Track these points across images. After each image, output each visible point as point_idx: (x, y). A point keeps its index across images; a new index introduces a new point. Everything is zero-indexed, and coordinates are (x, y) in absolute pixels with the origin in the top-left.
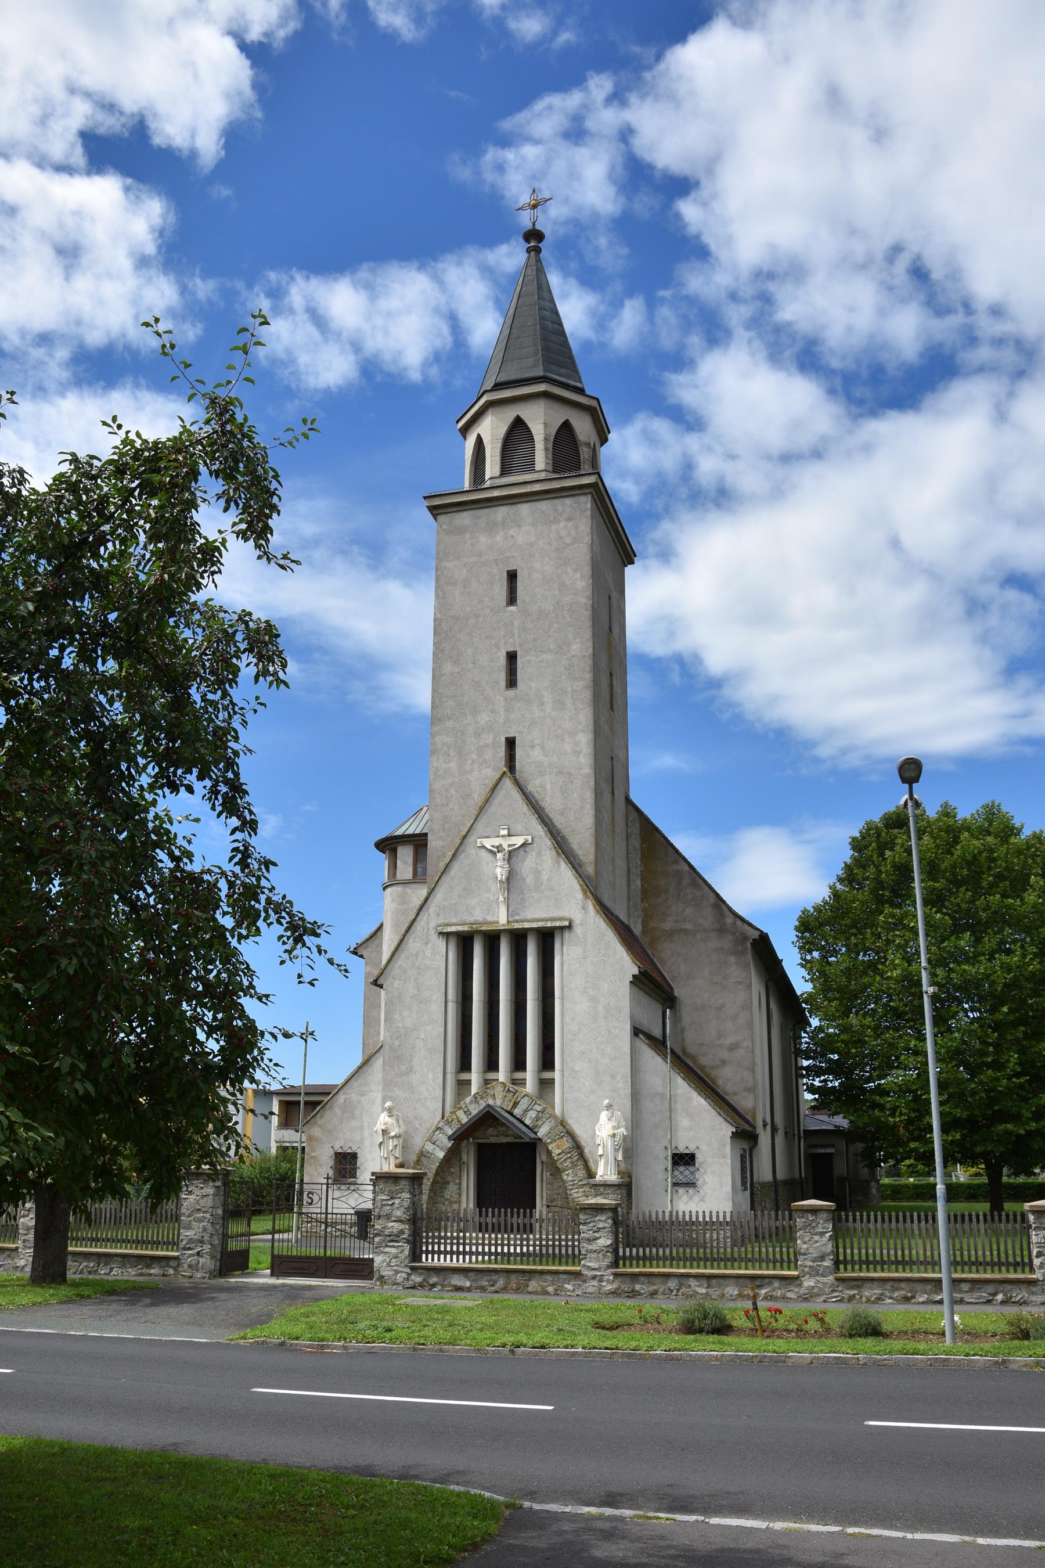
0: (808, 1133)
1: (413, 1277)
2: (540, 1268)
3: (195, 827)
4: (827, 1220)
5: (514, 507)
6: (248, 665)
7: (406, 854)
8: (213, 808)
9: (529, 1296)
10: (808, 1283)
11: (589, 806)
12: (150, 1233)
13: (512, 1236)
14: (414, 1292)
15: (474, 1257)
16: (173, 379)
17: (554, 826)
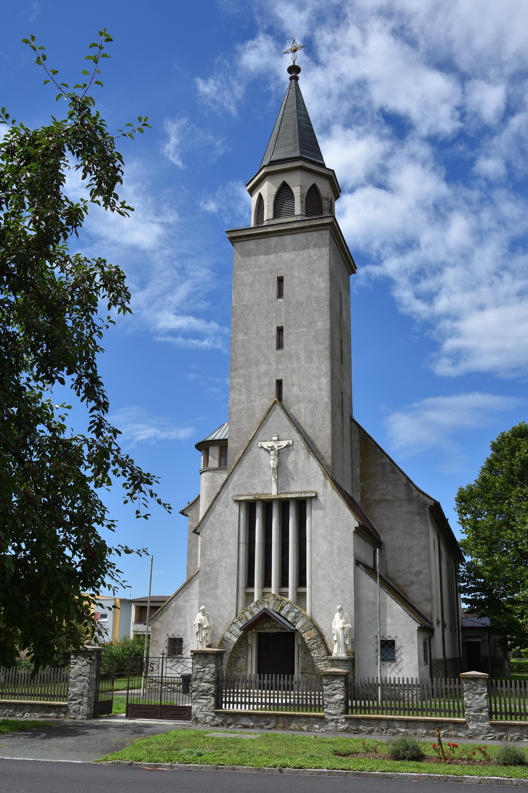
0: (464, 628)
1: (217, 719)
2: (298, 713)
3: (62, 401)
4: (483, 686)
5: (282, 238)
6: (103, 297)
7: (214, 452)
8: (78, 394)
9: (291, 732)
10: (472, 726)
11: (328, 422)
12: (32, 690)
13: (280, 692)
14: (217, 728)
15: (255, 706)
16: (45, 83)
17: (306, 435)
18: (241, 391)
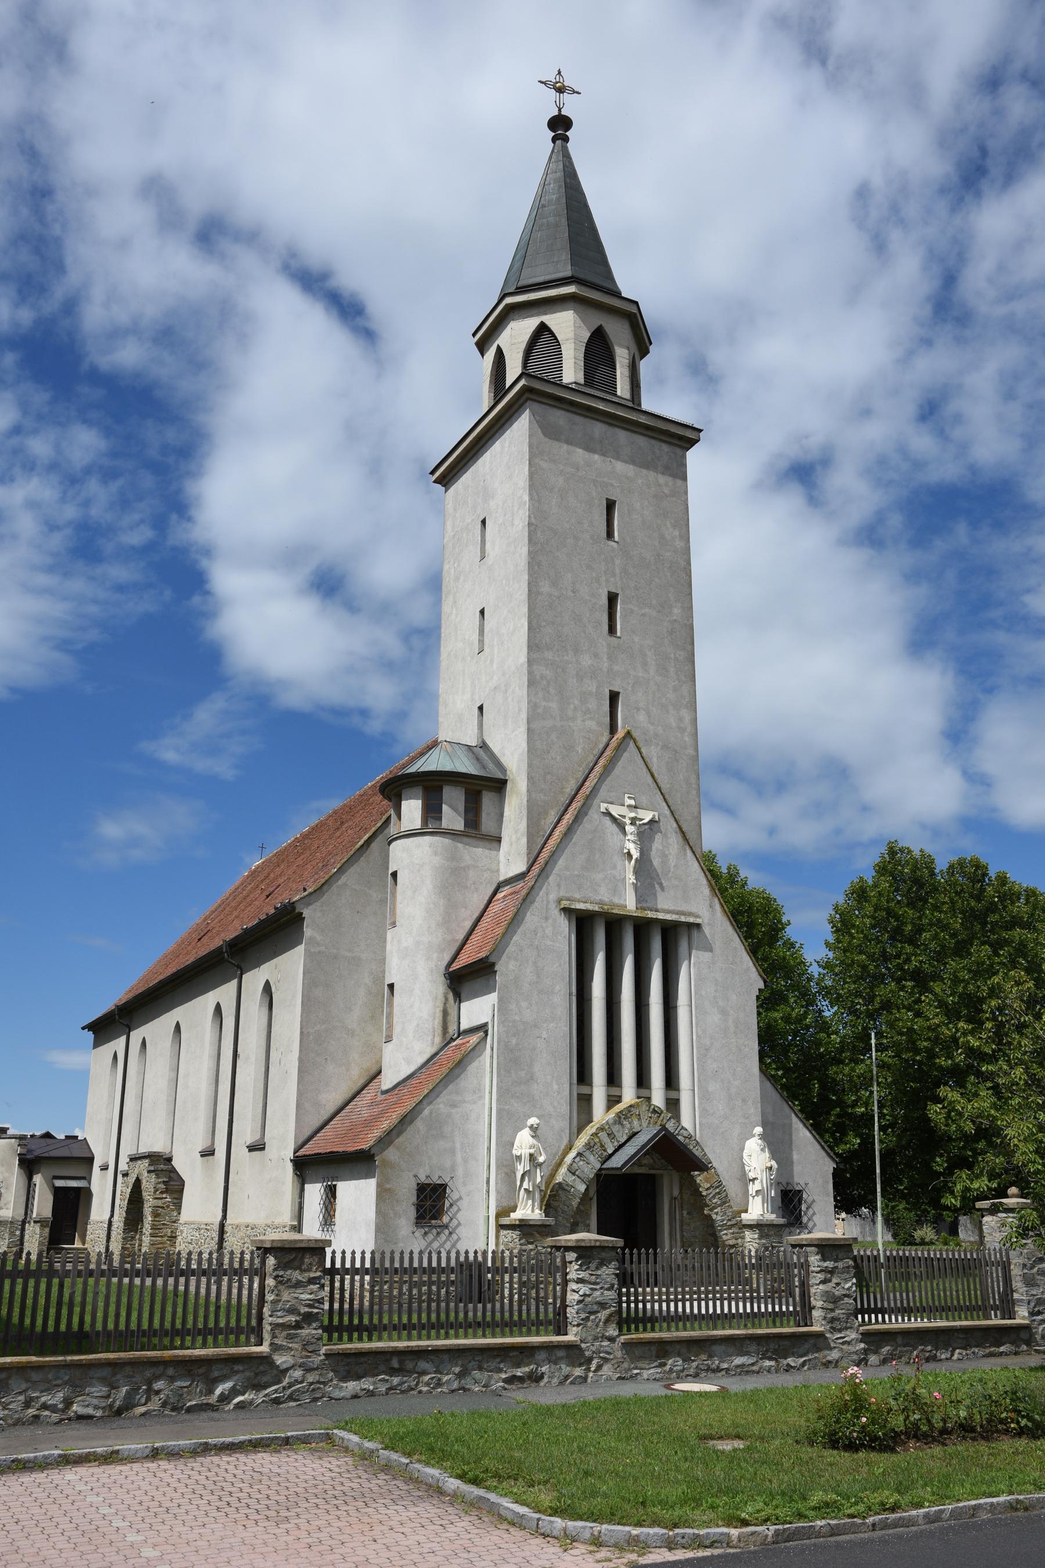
18: (548, 692)
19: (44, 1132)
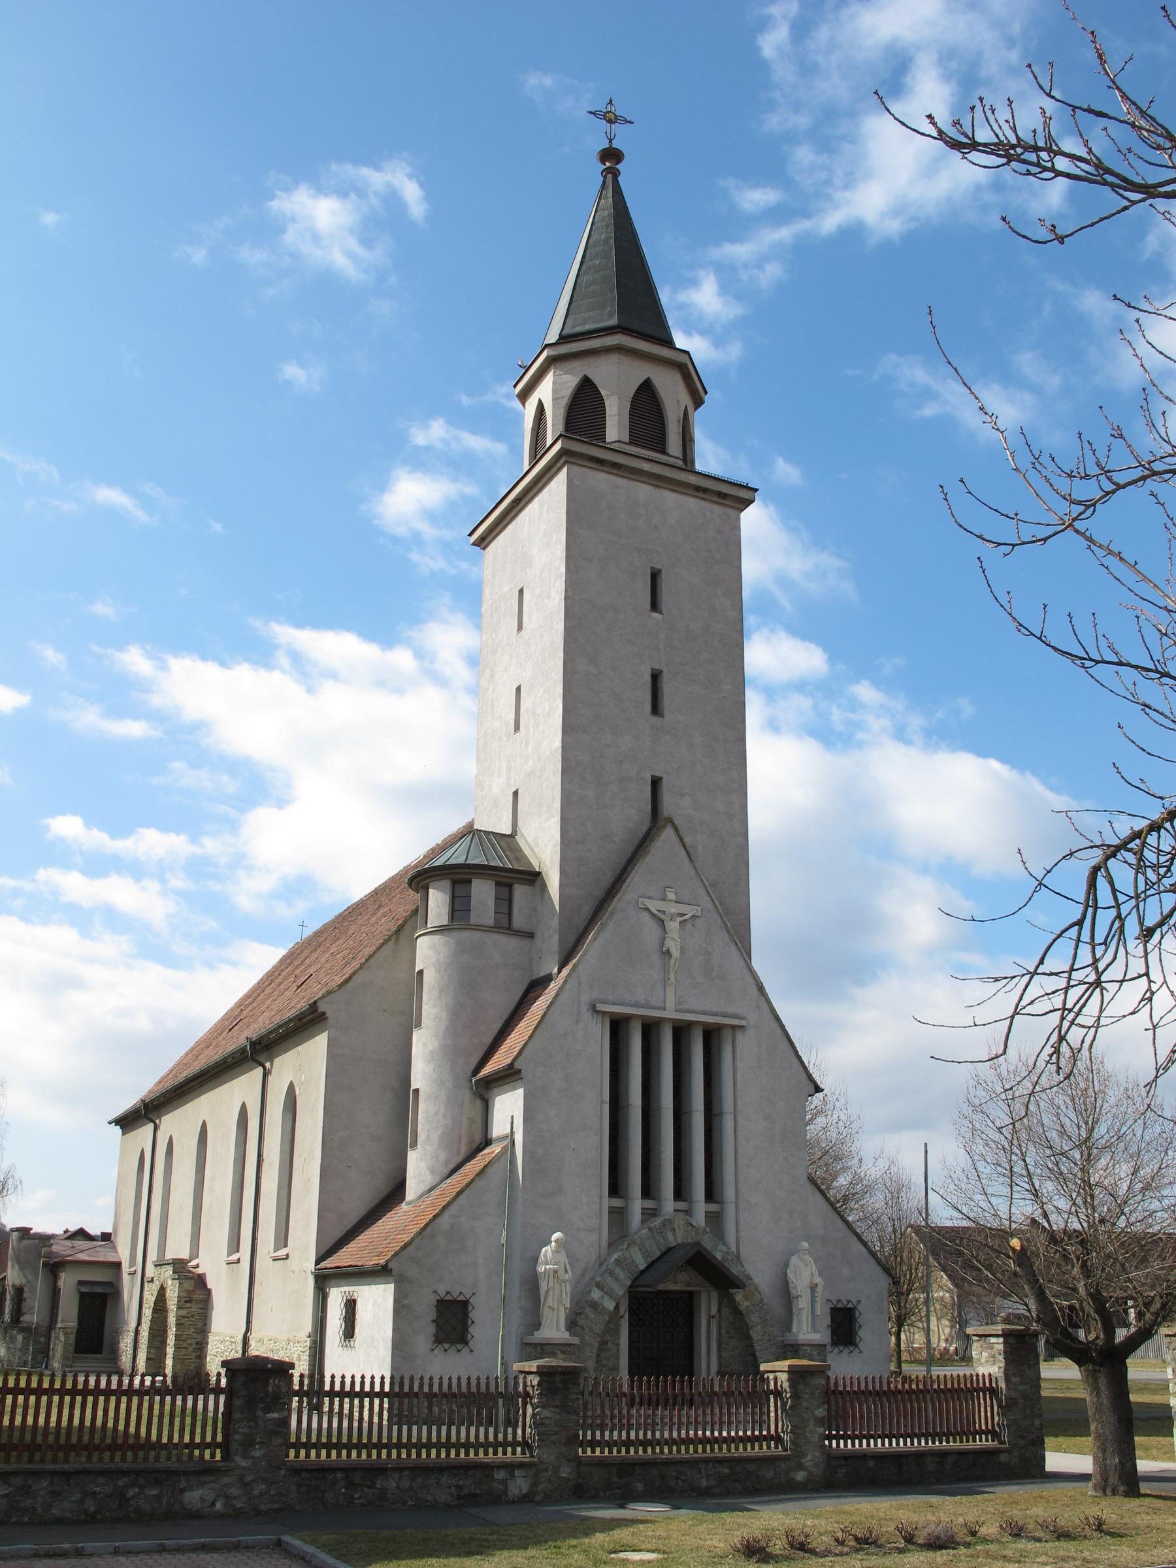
19: (78, 1227)
